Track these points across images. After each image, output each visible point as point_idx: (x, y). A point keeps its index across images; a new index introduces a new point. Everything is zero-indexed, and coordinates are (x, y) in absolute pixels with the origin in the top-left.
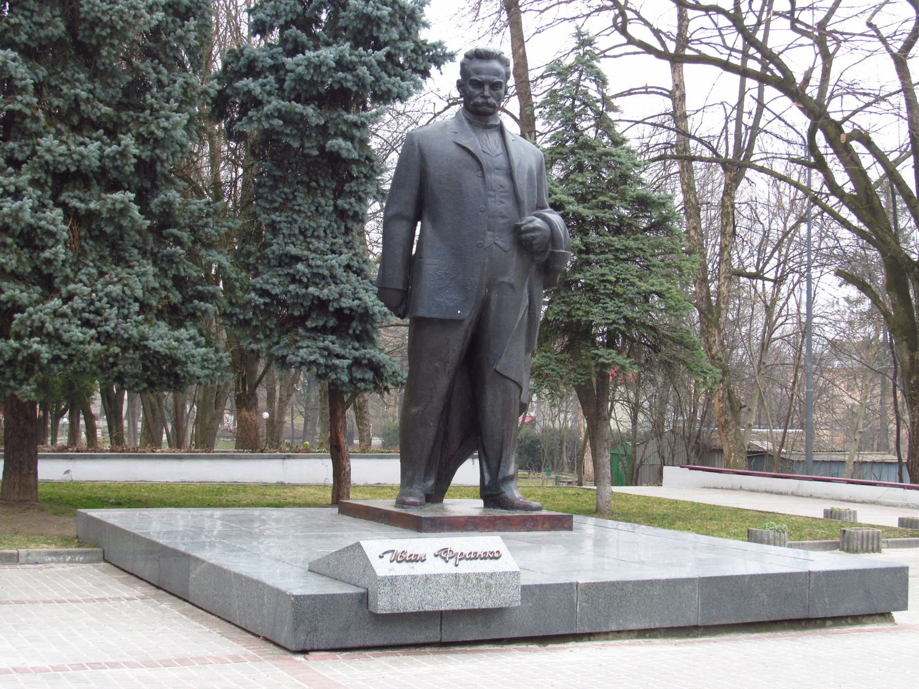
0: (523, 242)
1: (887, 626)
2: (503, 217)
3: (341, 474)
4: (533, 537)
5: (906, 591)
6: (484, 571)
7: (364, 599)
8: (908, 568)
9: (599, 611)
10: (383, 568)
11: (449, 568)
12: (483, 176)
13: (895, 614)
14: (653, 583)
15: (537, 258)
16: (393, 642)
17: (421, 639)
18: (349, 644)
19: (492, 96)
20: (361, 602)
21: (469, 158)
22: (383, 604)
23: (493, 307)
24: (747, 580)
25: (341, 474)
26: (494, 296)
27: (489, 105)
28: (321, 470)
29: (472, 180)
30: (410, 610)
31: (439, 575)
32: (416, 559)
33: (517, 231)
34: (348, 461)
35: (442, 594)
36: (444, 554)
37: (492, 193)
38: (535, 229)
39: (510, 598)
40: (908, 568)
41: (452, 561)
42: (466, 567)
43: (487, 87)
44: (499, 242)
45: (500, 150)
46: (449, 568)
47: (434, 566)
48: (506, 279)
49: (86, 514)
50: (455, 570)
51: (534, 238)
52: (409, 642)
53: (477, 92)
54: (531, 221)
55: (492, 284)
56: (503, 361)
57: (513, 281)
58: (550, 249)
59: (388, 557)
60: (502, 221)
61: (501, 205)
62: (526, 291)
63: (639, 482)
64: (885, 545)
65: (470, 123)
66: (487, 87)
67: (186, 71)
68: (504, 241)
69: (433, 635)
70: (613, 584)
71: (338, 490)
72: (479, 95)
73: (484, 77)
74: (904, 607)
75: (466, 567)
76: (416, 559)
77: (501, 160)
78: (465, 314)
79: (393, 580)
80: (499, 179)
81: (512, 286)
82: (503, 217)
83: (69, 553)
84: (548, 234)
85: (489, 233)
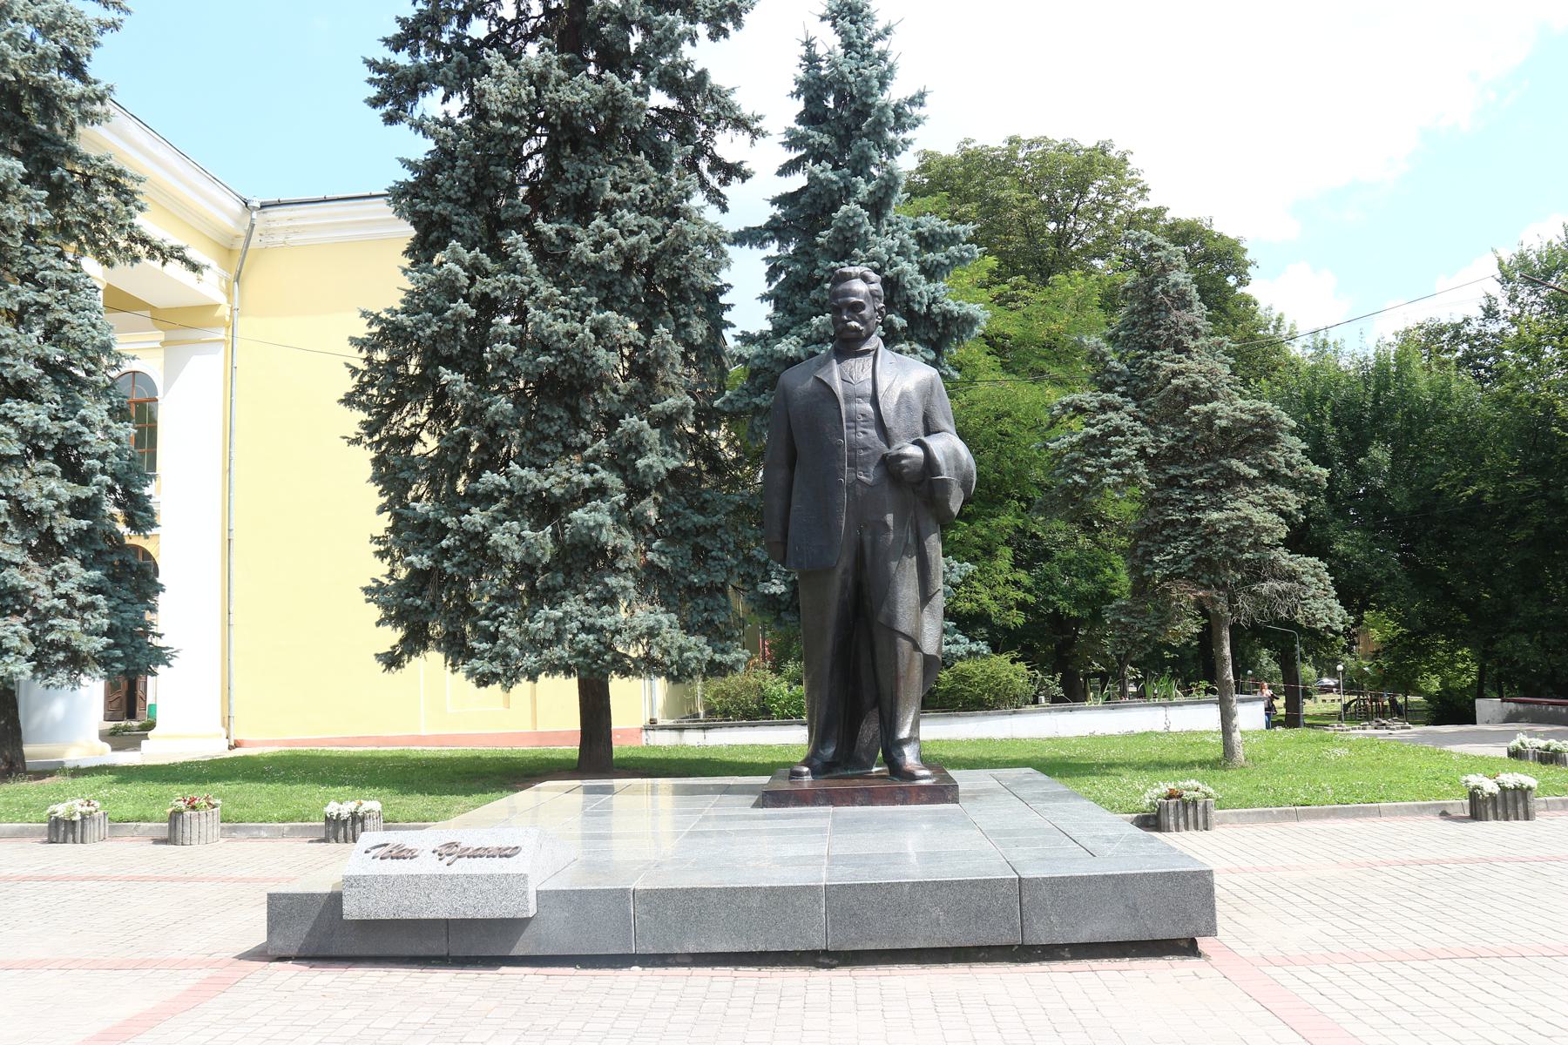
4: (936, 812)
6: (478, 872)
8: (1210, 872)
9: (669, 927)
11: (440, 868)
18: (334, 952)
24: (906, 889)
26: (867, 538)
30: (384, 917)
31: (418, 876)
35: (424, 899)
40: (272, 898)
42: (464, 867)
47: (427, 865)
64: (1543, 806)
67: (371, 435)
69: (437, 947)
70: (687, 892)
71: (1100, 766)
77: (869, 389)
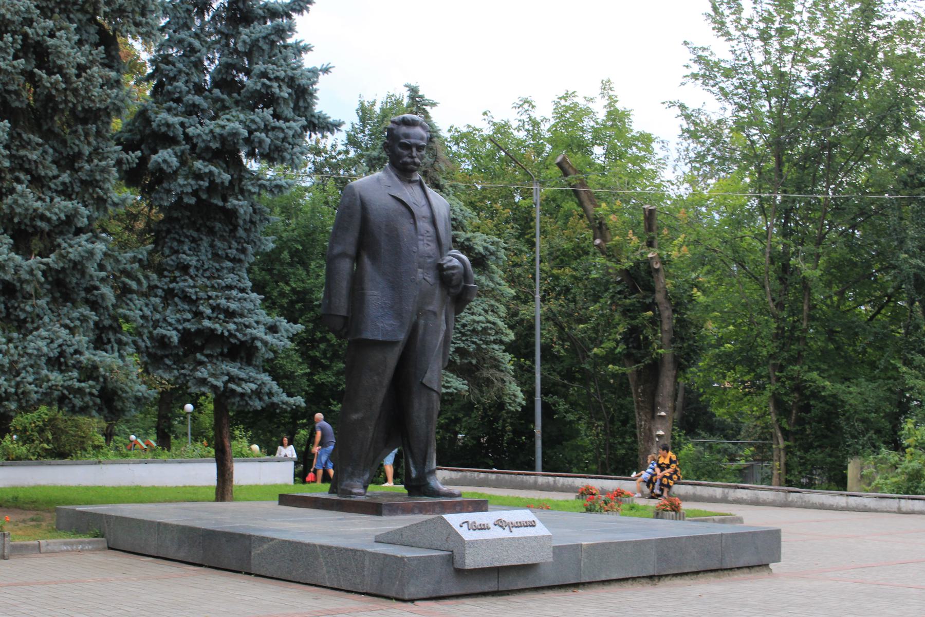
0: (443, 275)
1: (765, 573)
2: (430, 257)
3: (224, 475)
5: (779, 547)
7: (451, 559)
10: (467, 535)
11: (504, 534)
12: (415, 223)
13: (772, 566)
14: (627, 543)
15: (452, 290)
16: (469, 592)
17: (486, 588)
19: (418, 156)
20: (448, 561)
21: (402, 208)
22: (471, 562)
23: (421, 331)
25: (224, 475)
26: (422, 322)
27: (415, 163)
28: (205, 473)
29: (405, 226)
32: (484, 528)
33: (440, 268)
34: (232, 462)
36: (500, 524)
37: (420, 237)
38: (454, 268)
39: (543, 556)
41: (507, 528)
42: (518, 533)
43: (414, 149)
44: (427, 278)
45: (424, 202)
46: (504, 534)
47: (496, 533)
48: (431, 308)
49: (74, 510)
50: (511, 535)
51: (453, 274)
52: (478, 591)
53: (406, 152)
54: (451, 261)
55: (420, 311)
56: (428, 375)
57: (436, 310)
58: (463, 284)
59: (465, 525)
60: (429, 260)
61: (427, 247)
62: (443, 317)
63: (227, 497)
65: (399, 178)
66: (414, 149)
68: (430, 278)
69: (491, 586)
72: (407, 155)
73: (413, 141)
74: (778, 560)
75: (518, 533)
76: (484, 528)
78: (402, 337)
79: (473, 543)
80: (424, 226)
81: (435, 313)
82: (430, 257)
83: (80, 543)
84: (462, 271)
85: (420, 270)
